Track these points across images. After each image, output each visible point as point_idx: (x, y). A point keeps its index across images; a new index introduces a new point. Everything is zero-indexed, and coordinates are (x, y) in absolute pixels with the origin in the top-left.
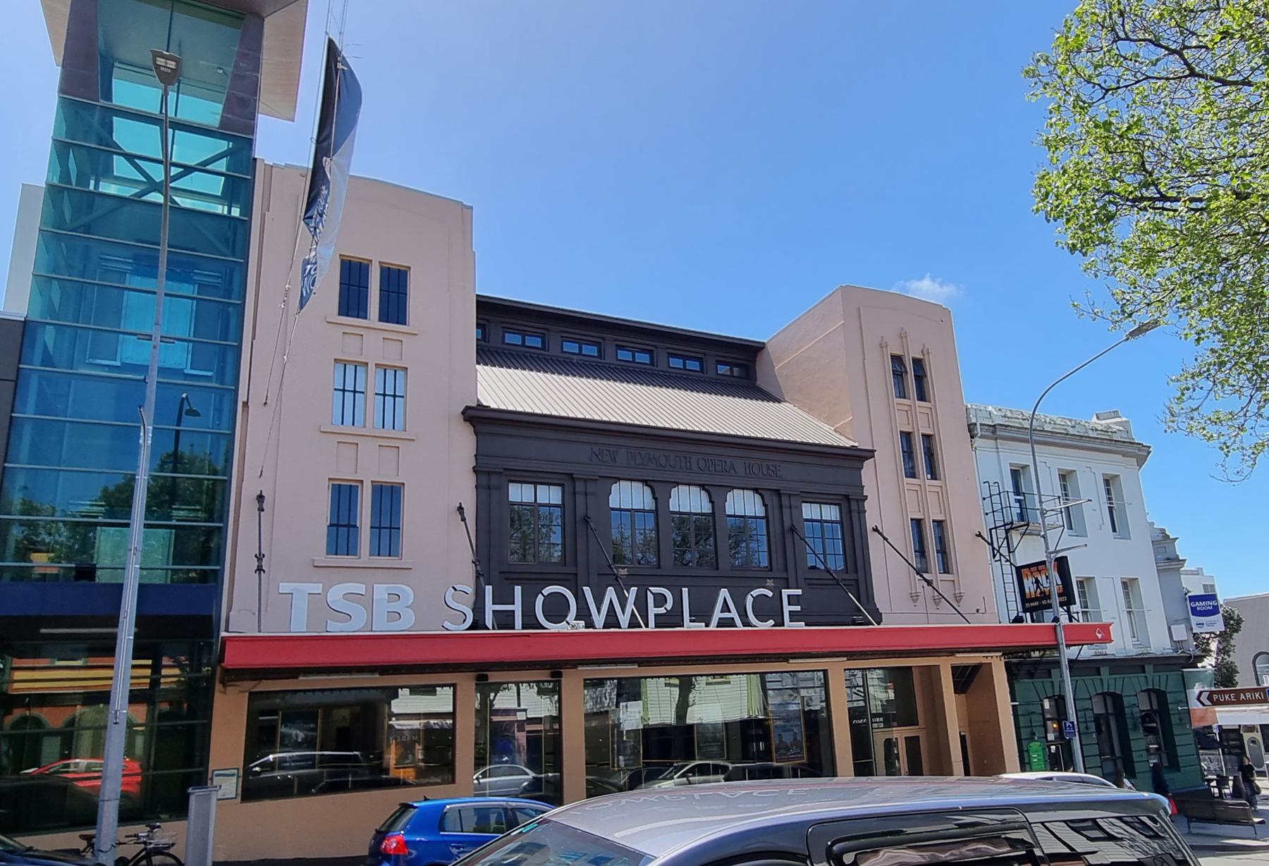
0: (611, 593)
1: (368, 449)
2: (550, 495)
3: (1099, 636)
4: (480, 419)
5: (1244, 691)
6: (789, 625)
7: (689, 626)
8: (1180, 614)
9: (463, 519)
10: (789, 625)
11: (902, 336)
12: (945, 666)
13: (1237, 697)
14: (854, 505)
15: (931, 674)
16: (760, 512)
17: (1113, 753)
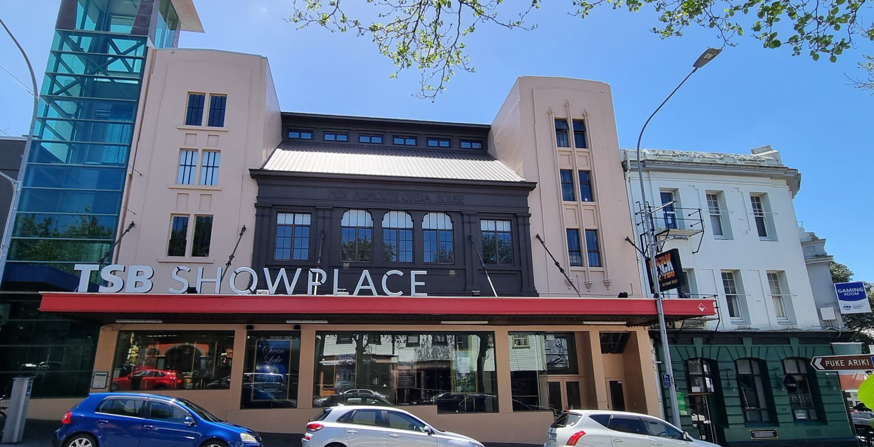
0: (283, 272)
1: (194, 197)
2: (304, 220)
3: (702, 309)
4: (261, 176)
5: (852, 358)
6: (414, 294)
7: (337, 293)
8: (828, 299)
9: (634, 245)
10: (414, 294)
11: (566, 106)
12: (594, 332)
13: (846, 363)
14: (520, 221)
15: (586, 335)
16: (449, 226)
17: (758, 405)
